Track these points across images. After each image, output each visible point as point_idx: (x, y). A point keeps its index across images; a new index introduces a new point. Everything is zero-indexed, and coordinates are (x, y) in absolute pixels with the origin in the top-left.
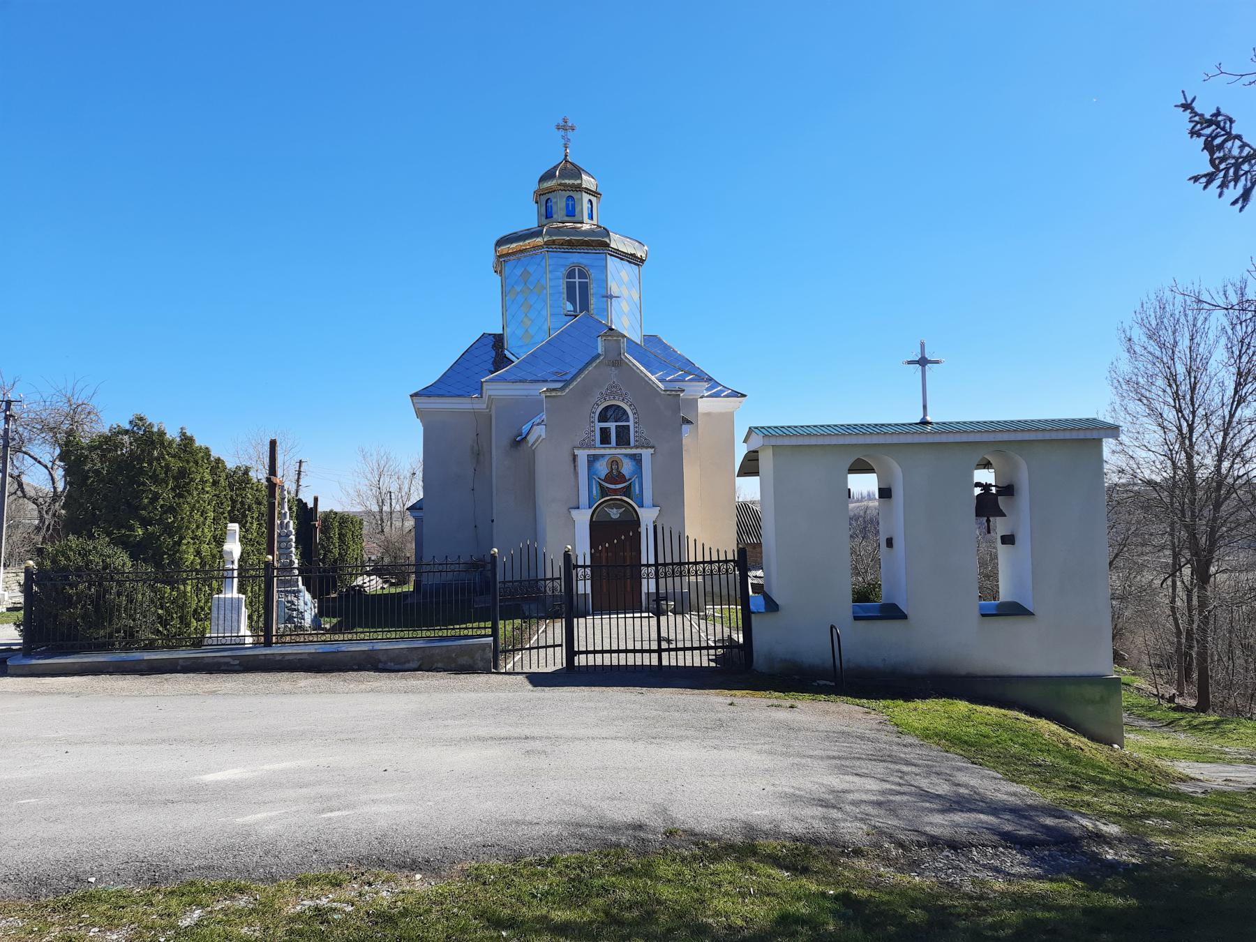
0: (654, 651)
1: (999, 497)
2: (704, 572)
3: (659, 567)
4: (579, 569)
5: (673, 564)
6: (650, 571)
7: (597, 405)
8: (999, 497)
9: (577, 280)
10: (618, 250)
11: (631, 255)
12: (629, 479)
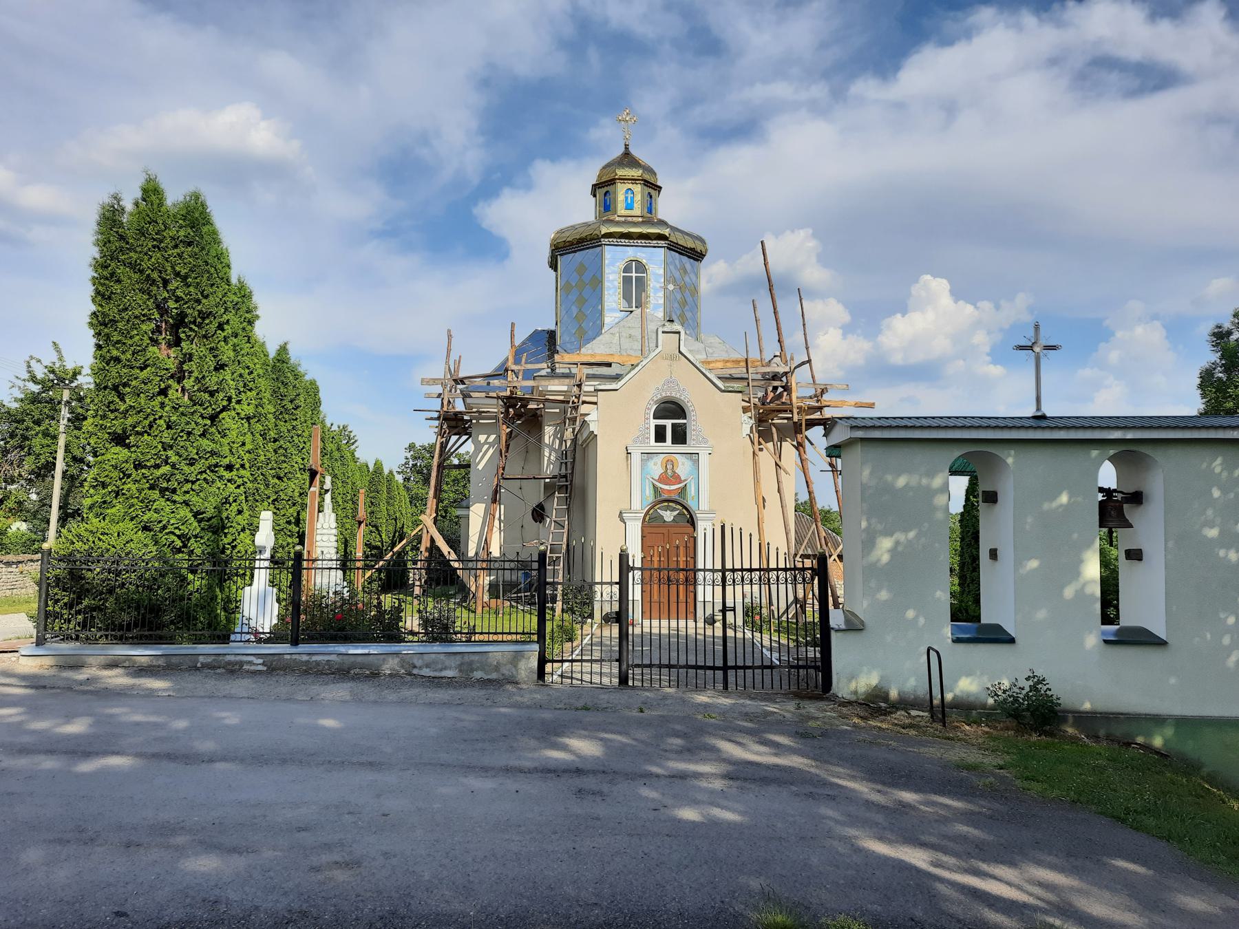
0: (718, 668)
1: (1124, 505)
2: (778, 580)
3: (727, 573)
4: (636, 572)
5: (742, 570)
6: (753, 576)
7: (648, 409)
8: (1124, 505)
9: (634, 275)
10: (677, 244)
11: (691, 249)
12: (685, 480)
